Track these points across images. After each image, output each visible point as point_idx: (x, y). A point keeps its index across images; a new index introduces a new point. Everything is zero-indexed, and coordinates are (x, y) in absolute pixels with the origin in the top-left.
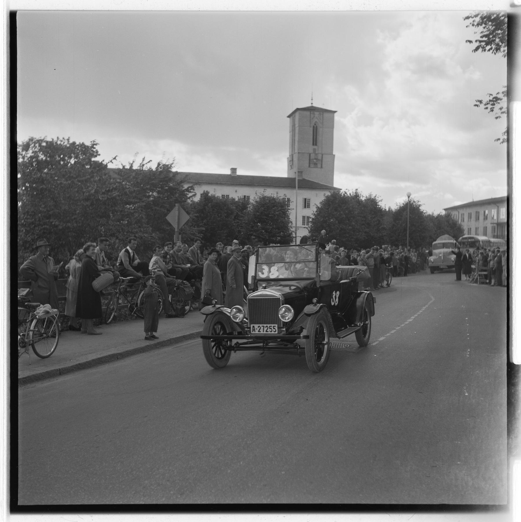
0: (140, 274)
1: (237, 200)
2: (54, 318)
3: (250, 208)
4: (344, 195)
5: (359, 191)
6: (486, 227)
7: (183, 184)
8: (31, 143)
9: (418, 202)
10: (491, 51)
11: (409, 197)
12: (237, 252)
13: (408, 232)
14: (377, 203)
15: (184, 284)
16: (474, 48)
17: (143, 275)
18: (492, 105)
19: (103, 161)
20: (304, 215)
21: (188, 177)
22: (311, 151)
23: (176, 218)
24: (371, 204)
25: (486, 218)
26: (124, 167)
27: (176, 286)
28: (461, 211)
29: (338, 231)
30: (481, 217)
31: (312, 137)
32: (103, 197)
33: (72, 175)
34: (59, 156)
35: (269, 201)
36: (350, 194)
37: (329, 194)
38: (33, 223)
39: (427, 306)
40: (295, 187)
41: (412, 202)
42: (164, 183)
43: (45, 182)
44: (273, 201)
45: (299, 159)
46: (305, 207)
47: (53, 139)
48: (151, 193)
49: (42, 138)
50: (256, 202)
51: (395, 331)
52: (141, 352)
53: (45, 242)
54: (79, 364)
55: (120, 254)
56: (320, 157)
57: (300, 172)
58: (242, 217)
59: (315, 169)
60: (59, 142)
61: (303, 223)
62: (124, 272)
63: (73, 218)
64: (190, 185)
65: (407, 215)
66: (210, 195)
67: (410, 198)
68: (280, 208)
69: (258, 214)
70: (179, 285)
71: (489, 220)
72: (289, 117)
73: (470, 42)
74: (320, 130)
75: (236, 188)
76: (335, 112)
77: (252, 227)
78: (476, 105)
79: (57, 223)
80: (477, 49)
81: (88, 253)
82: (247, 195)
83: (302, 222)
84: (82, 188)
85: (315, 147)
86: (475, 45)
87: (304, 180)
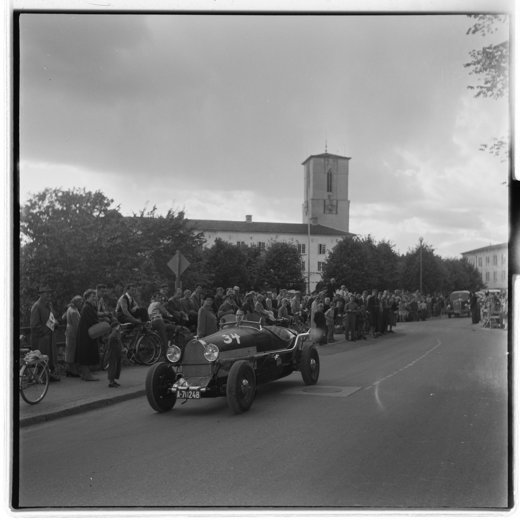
0: (138, 320)
1: (250, 246)
2: (44, 364)
3: (263, 255)
4: (356, 240)
5: (372, 237)
7: (193, 231)
8: (47, 193)
10: (493, 96)
11: (421, 242)
15: (183, 329)
17: (142, 321)
20: (320, 261)
21: (198, 224)
23: (177, 264)
26: (135, 215)
27: (175, 332)
29: (351, 276)
32: (107, 245)
33: (76, 223)
34: (76, 206)
35: (282, 247)
36: (363, 240)
37: (342, 240)
38: (37, 271)
39: (431, 350)
41: (424, 247)
42: (176, 231)
43: (50, 231)
44: (285, 248)
45: (313, 206)
46: (320, 253)
48: (161, 241)
49: (58, 189)
52: (132, 398)
53: (48, 288)
54: (67, 410)
55: (119, 301)
56: (334, 203)
57: (314, 218)
58: (254, 263)
59: (330, 215)
60: (75, 193)
62: (122, 318)
63: (77, 265)
64: (200, 232)
65: (420, 259)
67: (422, 243)
68: (292, 254)
69: (270, 260)
70: (178, 330)
73: (472, 88)
74: (335, 177)
75: (251, 235)
76: (349, 159)
77: (265, 273)
79: (61, 271)
80: (479, 94)
81: (89, 300)
82: (262, 241)
83: (317, 268)
85: (330, 193)
87: (319, 226)
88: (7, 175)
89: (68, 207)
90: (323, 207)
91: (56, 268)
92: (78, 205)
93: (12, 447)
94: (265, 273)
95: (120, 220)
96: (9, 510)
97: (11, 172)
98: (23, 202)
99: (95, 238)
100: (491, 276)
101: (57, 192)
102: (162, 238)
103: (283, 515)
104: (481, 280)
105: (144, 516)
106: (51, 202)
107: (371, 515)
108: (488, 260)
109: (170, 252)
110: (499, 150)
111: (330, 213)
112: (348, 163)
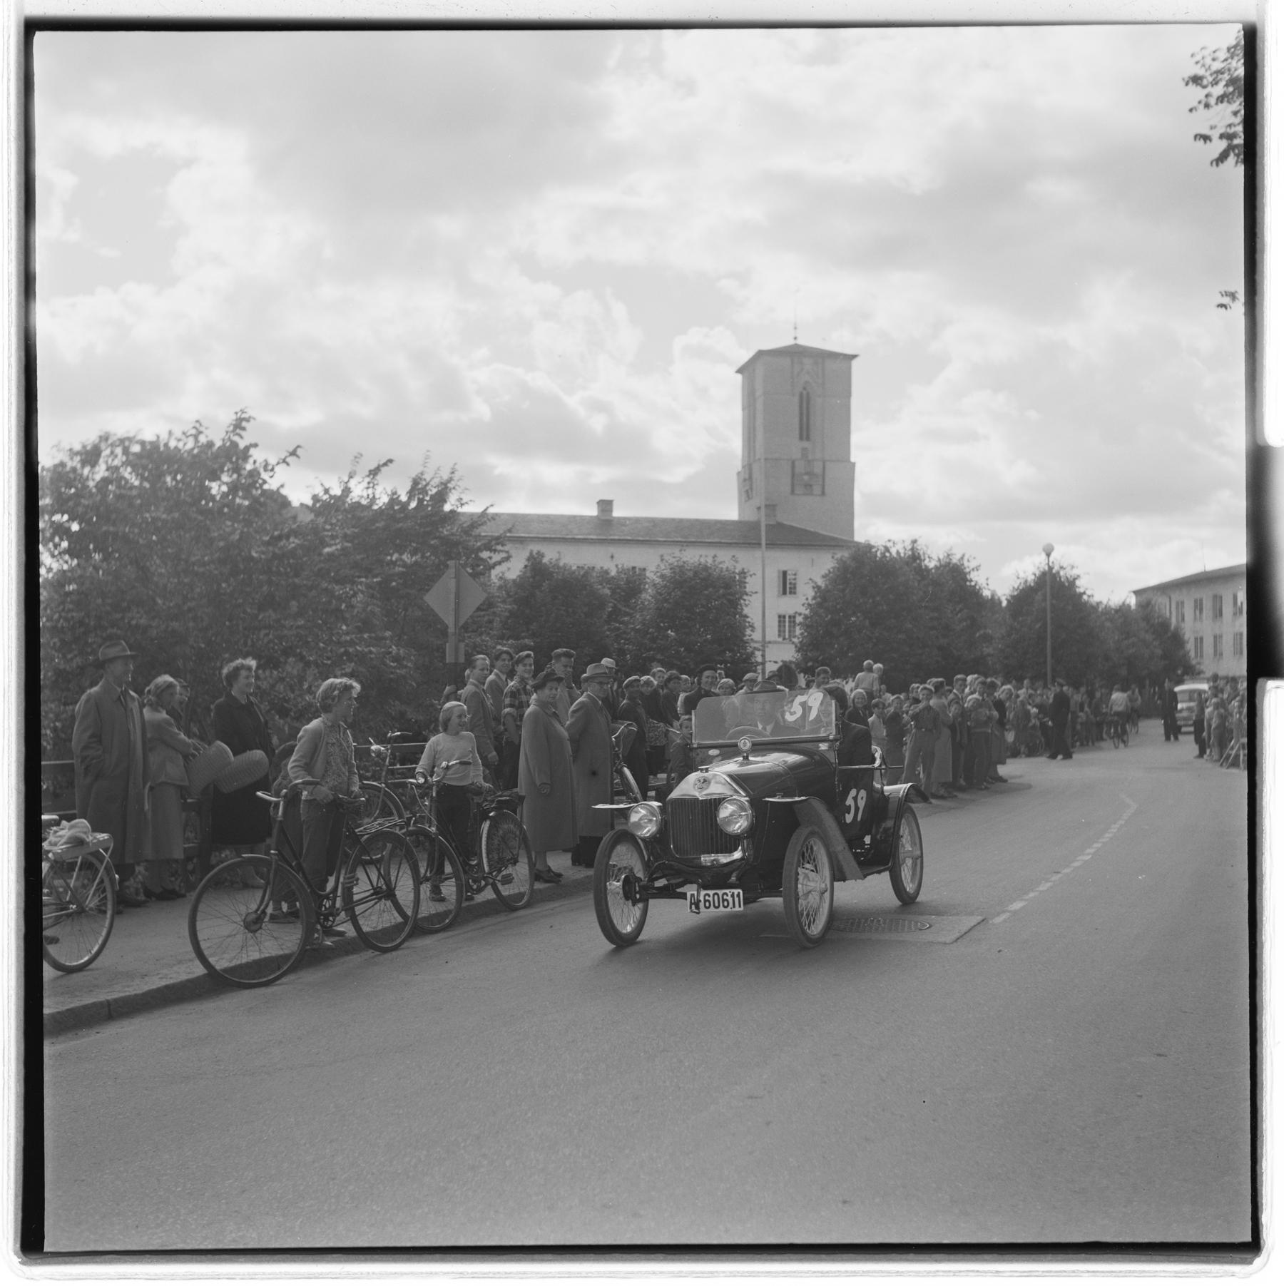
2: (100, 858)
3: (647, 596)
4: (883, 555)
5: (921, 546)
8: (103, 446)
9: (1073, 567)
11: (1048, 555)
12: (601, 683)
13: (1049, 643)
14: (965, 574)
16: (1216, 155)
19: (282, 486)
20: (782, 613)
24: (952, 583)
28: (1176, 597)
31: (796, 420)
34: (174, 478)
35: (696, 573)
36: (898, 552)
38: (81, 623)
40: (759, 544)
46: (784, 593)
49: (131, 435)
50: (662, 576)
51: (1049, 884)
54: (167, 987)
56: (817, 469)
57: (771, 508)
58: (627, 614)
60: (172, 444)
61: (781, 632)
65: (1044, 600)
66: (545, 560)
68: (721, 591)
72: (739, 371)
73: (1206, 138)
75: (612, 549)
76: (854, 356)
79: (143, 621)
83: (776, 629)
84: (208, 530)
85: (806, 444)
86: (1219, 146)
87: (780, 525)
88: (9, 432)
89: (157, 477)
91: (130, 615)
92: (179, 477)
93: (22, 1104)
94: (654, 640)
96: (16, 1260)
97: (18, 421)
98: (46, 459)
99: (233, 532)
101: (127, 443)
103: (693, 1272)
104: (1186, 655)
105: (349, 1276)
106: (112, 469)
107: (909, 1273)
108: (1199, 606)
109: (421, 579)
111: (805, 494)
112: (850, 368)
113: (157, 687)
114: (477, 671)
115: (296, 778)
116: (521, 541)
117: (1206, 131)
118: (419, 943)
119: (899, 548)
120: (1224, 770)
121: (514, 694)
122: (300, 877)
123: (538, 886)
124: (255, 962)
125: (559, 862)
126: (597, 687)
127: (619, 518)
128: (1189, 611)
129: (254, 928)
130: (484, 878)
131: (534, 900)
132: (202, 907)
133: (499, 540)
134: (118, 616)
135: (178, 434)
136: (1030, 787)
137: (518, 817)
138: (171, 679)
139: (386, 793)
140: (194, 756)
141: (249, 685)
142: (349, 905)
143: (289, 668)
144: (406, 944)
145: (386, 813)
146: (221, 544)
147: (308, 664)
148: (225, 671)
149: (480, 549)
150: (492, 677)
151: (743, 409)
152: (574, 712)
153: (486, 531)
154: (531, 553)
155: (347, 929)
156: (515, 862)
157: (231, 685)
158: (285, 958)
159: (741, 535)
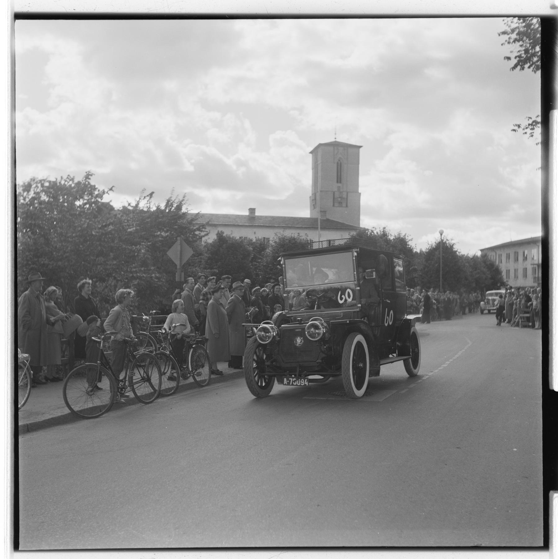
1: (254, 240)
3: (269, 251)
4: (371, 233)
5: (387, 230)
6: (526, 269)
8: (32, 183)
9: (452, 240)
11: (441, 235)
12: (240, 290)
13: (441, 273)
14: (406, 242)
16: (513, 66)
18: (532, 129)
22: (335, 189)
24: (401, 246)
25: (525, 259)
28: (498, 252)
30: (521, 258)
31: (335, 175)
34: (63, 197)
35: (290, 241)
36: (377, 233)
44: (293, 241)
47: (57, 179)
49: (45, 178)
50: (275, 242)
54: (52, 418)
56: (344, 195)
57: (323, 212)
60: (63, 182)
65: (439, 254)
66: (224, 235)
67: (443, 236)
71: (529, 261)
73: (509, 58)
75: (255, 230)
78: (514, 130)
79: (46, 262)
82: (266, 237)
85: (339, 185)
86: (514, 61)
87: (328, 220)
89: (55, 198)
90: (332, 199)
94: (271, 270)
95: (113, 212)
99: (84, 224)
100: (512, 274)
101: (43, 182)
102: (160, 230)
104: (501, 278)
106: (37, 193)
108: (508, 257)
109: (169, 243)
110: (533, 131)
113: (49, 292)
114: (189, 284)
115: (108, 330)
116: (215, 226)
117: (508, 55)
118: (160, 400)
119: (378, 231)
120: (513, 328)
121: (205, 295)
122: (110, 372)
123: (213, 376)
124: (90, 408)
125: (223, 367)
126: (239, 291)
127: (258, 216)
128: (504, 259)
129: (90, 394)
130: (189, 373)
131: (210, 382)
132: (68, 384)
133: (203, 226)
134: (36, 260)
135: (65, 177)
136: (428, 335)
137: (205, 347)
138: (54, 288)
139: (149, 337)
140: (66, 321)
141: (89, 290)
142: (132, 384)
143: (110, 282)
144: (156, 401)
145: (149, 345)
146: (80, 229)
147: (118, 281)
148: (79, 285)
149: (195, 230)
150: (197, 286)
151: (313, 169)
152: (229, 303)
153: (200, 221)
154: (218, 231)
155: (131, 395)
156: (203, 366)
157: (81, 291)
158: (104, 406)
159: (308, 224)
